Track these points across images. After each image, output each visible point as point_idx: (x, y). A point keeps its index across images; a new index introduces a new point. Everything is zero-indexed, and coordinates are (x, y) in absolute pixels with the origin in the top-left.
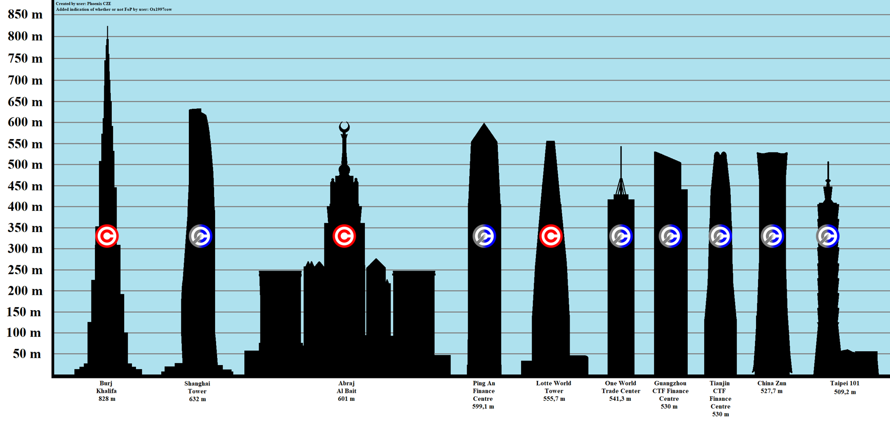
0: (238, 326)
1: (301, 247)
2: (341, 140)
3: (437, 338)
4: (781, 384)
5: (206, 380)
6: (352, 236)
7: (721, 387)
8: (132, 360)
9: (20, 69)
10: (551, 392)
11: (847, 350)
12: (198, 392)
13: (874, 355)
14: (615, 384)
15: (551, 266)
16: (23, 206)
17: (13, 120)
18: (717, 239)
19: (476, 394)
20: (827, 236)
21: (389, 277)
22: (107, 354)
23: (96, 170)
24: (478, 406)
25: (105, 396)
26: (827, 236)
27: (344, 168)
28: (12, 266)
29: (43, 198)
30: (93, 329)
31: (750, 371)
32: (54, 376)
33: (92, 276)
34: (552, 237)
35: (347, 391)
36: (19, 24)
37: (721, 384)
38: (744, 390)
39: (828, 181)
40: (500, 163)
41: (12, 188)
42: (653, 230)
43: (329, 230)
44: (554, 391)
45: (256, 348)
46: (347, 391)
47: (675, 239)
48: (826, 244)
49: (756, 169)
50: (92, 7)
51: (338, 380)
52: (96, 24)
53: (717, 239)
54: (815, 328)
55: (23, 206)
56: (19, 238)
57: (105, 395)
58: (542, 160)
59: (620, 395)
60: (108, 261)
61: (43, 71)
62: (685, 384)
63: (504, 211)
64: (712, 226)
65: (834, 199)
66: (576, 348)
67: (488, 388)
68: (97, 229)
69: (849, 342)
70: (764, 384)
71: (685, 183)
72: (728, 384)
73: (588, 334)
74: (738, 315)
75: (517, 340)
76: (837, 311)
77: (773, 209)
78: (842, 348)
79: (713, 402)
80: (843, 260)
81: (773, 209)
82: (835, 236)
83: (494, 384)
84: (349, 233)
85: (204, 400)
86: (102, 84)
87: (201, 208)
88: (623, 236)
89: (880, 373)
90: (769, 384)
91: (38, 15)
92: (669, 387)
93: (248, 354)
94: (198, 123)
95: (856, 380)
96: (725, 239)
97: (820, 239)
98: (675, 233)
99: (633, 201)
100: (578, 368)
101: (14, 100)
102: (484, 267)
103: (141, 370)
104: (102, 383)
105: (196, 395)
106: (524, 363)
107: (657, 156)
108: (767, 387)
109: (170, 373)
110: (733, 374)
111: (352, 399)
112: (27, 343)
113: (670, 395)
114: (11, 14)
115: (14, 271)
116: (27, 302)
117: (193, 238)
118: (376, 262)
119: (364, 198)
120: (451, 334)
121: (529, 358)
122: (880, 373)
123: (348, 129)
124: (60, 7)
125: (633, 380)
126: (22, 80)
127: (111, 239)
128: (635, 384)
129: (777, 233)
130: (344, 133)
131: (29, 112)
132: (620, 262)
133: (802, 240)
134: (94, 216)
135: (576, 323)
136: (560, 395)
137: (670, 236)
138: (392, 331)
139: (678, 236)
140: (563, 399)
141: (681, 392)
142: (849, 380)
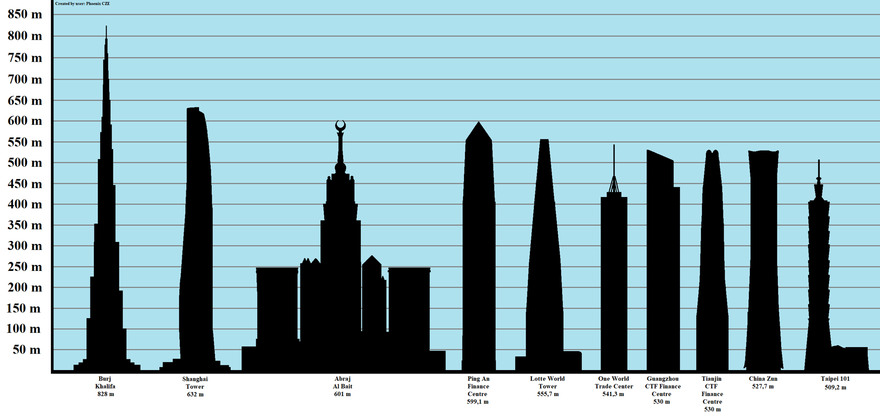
0: (236, 322)
1: (299, 244)
2: (337, 138)
3: (433, 334)
4: (772, 379)
5: (203, 376)
7: (712, 382)
8: (131, 356)
9: (20, 68)
10: (545, 387)
11: (838, 346)
12: (195, 387)
13: (864, 351)
14: (608, 379)
16: (23, 204)
17: (13, 118)
19: (471, 389)
21: (385, 274)
22: (106, 350)
23: (95, 168)
24: (472, 401)
25: (104, 391)
27: (340, 166)
28: (12, 263)
29: (43, 195)
30: (92, 325)
31: (741, 367)
32: (53, 372)
33: (91, 273)
35: (343, 386)
36: (18, 24)
37: (713, 379)
38: (736, 386)
39: (819, 179)
40: (494, 161)
41: (12, 186)
44: (548, 387)
45: (253, 344)
46: (343, 386)
49: (747, 167)
51: (334, 376)
54: (806, 324)
55: (23, 204)
56: (19, 235)
57: (104, 390)
58: (536, 158)
59: (613, 390)
61: (43, 70)
62: (677, 379)
63: (498, 209)
65: (825, 197)
66: (569, 344)
67: (482, 383)
69: (840, 338)
70: (755, 379)
71: (677, 181)
72: (720, 379)
73: (581, 330)
74: (729, 311)
75: (511, 336)
76: (827, 307)
78: (833, 344)
79: (705, 397)
83: (488, 379)
85: (201, 395)
86: (101, 83)
89: (871, 368)
90: (760, 379)
91: (37, 15)
92: (661, 382)
93: (245, 350)
94: (196, 122)
95: (847, 375)
99: (626, 198)
100: (571, 363)
101: (13, 98)
103: (139, 366)
104: (101, 379)
105: (194, 390)
106: (518, 359)
107: (650, 154)
108: (758, 382)
109: (168, 368)
110: (725, 369)
111: (348, 395)
112: (26, 339)
113: (663, 391)
114: (11, 13)
115: (14, 267)
116: (27, 298)
118: (372, 259)
119: (360, 196)
120: (446, 330)
121: (523, 354)
122: (871, 368)
123: (344, 128)
125: (626, 375)
126: (22, 79)
128: (627, 379)
130: (340, 131)
131: (29, 111)
135: (569, 319)
136: (554, 391)
138: (388, 327)
140: (556, 395)
141: (673, 387)
142: (840, 375)
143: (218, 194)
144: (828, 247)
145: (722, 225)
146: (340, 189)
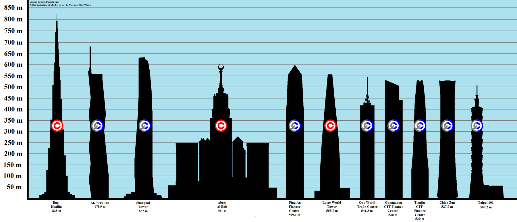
0: (165, 171)
1: (198, 131)
2: (219, 74)
3: (342, 179)
4: (452, 203)
5: (147, 201)
6: (225, 126)
7: (420, 205)
8: (70, 190)
9: (11, 37)
10: (330, 207)
11: (487, 185)
12: (143, 207)
13: (501, 188)
15: (330, 142)
16: (12, 109)
17: (7, 63)
18: (418, 127)
19: (291, 208)
20: (476, 125)
21: (245, 147)
25: (56, 209)
26: (476, 125)
27: (221, 89)
28: (6, 141)
29: (23, 104)
30: (50, 174)
31: (435, 196)
32: (28, 199)
34: (331, 126)
35: (222, 207)
36: (10, 13)
37: (420, 203)
38: (432, 207)
39: (477, 96)
40: (303, 86)
41: (6, 99)
42: (384, 122)
43: (213, 122)
44: (332, 207)
45: (174, 184)
46: (222, 207)
47: (297, 127)
48: (476, 130)
49: (438, 89)
50: (49, 4)
51: (218, 201)
52: (51, 13)
53: (418, 127)
54: (470, 173)
55: (12, 109)
56: (10, 126)
57: (56, 209)
59: (367, 209)
60: (57, 139)
62: (401, 203)
63: (305, 112)
64: (473, 119)
65: (480, 105)
66: (344, 184)
67: (297, 205)
68: (52, 121)
69: (488, 181)
70: (443, 203)
71: (401, 97)
72: (424, 203)
73: (350, 176)
74: (429, 166)
75: (312, 180)
77: (448, 111)
78: (484, 184)
79: (416, 213)
80: (485, 137)
81: (448, 111)
82: (481, 126)
83: (300, 203)
84: (223, 124)
85: (146, 211)
86: (54, 44)
87: (145, 110)
88: (449, 126)
89: (505, 197)
90: (446, 203)
91: (20, 8)
92: (392, 204)
93: (170, 187)
94: (143, 64)
95: (492, 201)
96: (422, 127)
97: (473, 127)
98: (297, 124)
99: (374, 106)
101: (7, 53)
102: (295, 143)
104: (54, 203)
105: (142, 209)
107: (386, 82)
108: (445, 205)
109: (129, 197)
110: (427, 198)
111: (225, 211)
113: (393, 209)
114: (6, 7)
115: (8, 143)
116: (14, 159)
117: (141, 127)
119: (231, 105)
120: (277, 176)
121: (319, 189)
122: (505, 197)
124: (31, 4)
125: (374, 201)
126: (12, 42)
127: (59, 127)
129: (450, 124)
131: (16, 59)
132: (367, 140)
133: (463, 127)
134: (50, 115)
135: (344, 171)
136: (335, 209)
137: (393, 125)
138: (246, 175)
139: (299, 126)
140: (336, 211)
141: (399, 207)
142: (488, 201)
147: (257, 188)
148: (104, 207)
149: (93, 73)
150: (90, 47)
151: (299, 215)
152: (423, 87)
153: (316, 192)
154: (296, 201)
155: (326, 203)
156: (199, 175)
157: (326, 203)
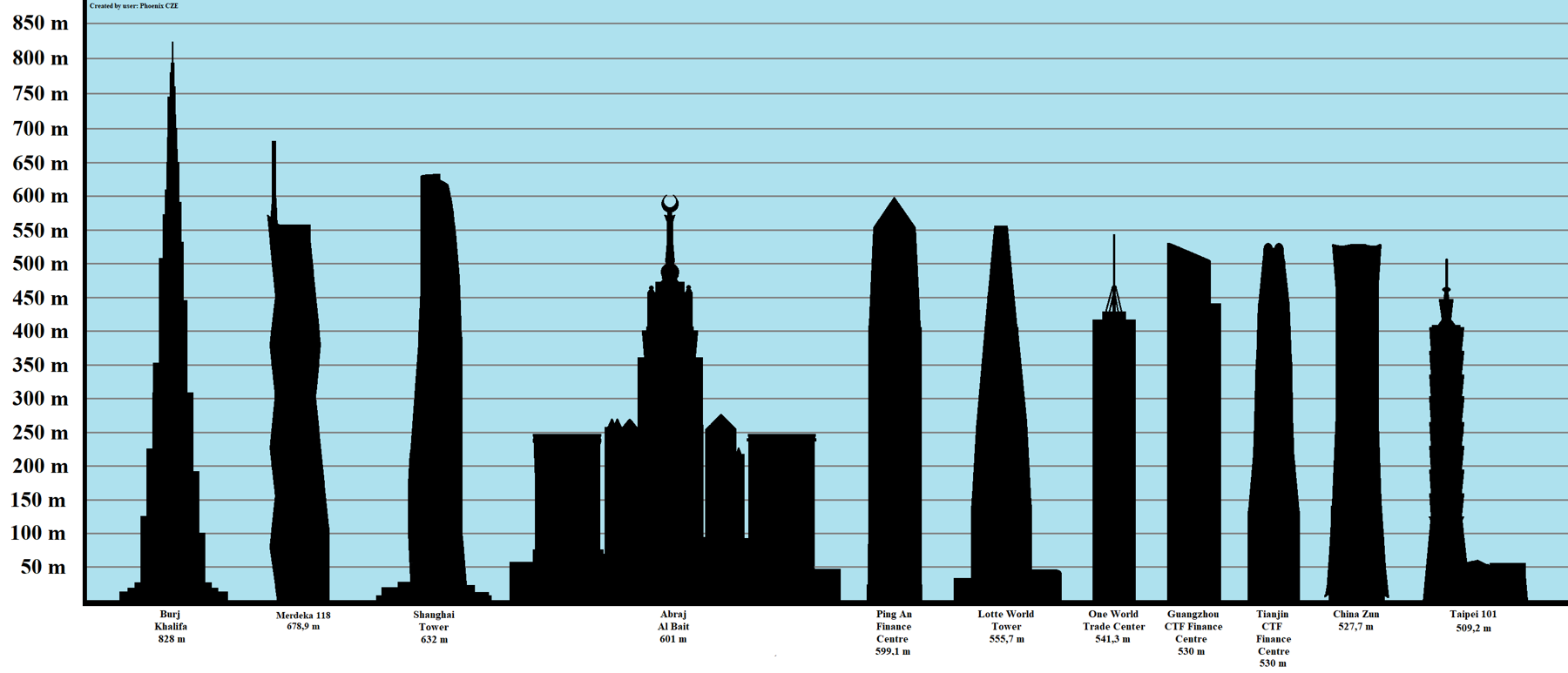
0: (500, 520)
2: (664, 224)
3: (1037, 543)
4: (1371, 615)
5: (447, 609)
7: (1274, 620)
8: (213, 577)
9: (33, 111)
10: (1001, 627)
11: (1478, 562)
12: (435, 627)
13: (1520, 569)
16: (37, 330)
17: (22, 192)
19: (881, 632)
21: (743, 445)
25: (169, 635)
27: (670, 269)
28: (19, 427)
29: (70, 317)
30: (150, 529)
31: (1321, 595)
32: (86, 603)
35: (674, 626)
36: (30, 40)
37: (1274, 615)
38: (1312, 627)
39: (1446, 290)
40: (919, 260)
41: (20, 301)
44: (1007, 627)
45: (528, 557)
46: (674, 626)
49: (1330, 271)
51: (660, 609)
54: (1425, 525)
55: (37, 330)
56: (31, 381)
57: (169, 633)
59: (1112, 633)
62: (1216, 615)
63: (926, 339)
65: (1457, 319)
66: (1042, 557)
67: (900, 621)
69: (1479, 549)
70: (1343, 615)
71: (1217, 293)
72: (1286, 615)
73: (1061, 535)
74: (1301, 504)
75: (947, 547)
78: (1469, 559)
79: (1261, 644)
83: (910, 615)
85: (444, 640)
86: (165, 133)
89: (1530, 597)
90: (1351, 615)
91: (60, 25)
92: (1190, 620)
93: (515, 567)
94: (435, 195)
95: (1492, 608)
99: (1133, 322)
101: (22, 160)
104: (163, 614)
105: (432, 633)
107: (1172, 248)
108: (1349, 620)
109: (390, 597)
110: (1295, 600)
111: (683, 640)
113: (1193, 633)
114: (17, 22)
115: (23, 434)
116: (43, 482)
119: (701, 318)
120: (841, 534)
121: (967, 574)
122: (1530, 597)
125: (1134, 609)
126: (35, 128)
131: (47, 180)
135: (1042, 517)
136: (1017, 634)
138: (746, 530)
140: (1020, 640)
141: (1210, 627)
142: (1480, 609)
143: (471, 315)
144: (1460, 401)
145: (1289, 365)
146: (670, 307)
147: (780, 571)
148: (316, 627)
149: (281, 221)
150: (274, 143)
151: (906, 652)
152: (1283, 263)
153: (957, 582)
154: (898, 609)
155: (987, 615)
156: (602, 529)
157: (987, 615)
